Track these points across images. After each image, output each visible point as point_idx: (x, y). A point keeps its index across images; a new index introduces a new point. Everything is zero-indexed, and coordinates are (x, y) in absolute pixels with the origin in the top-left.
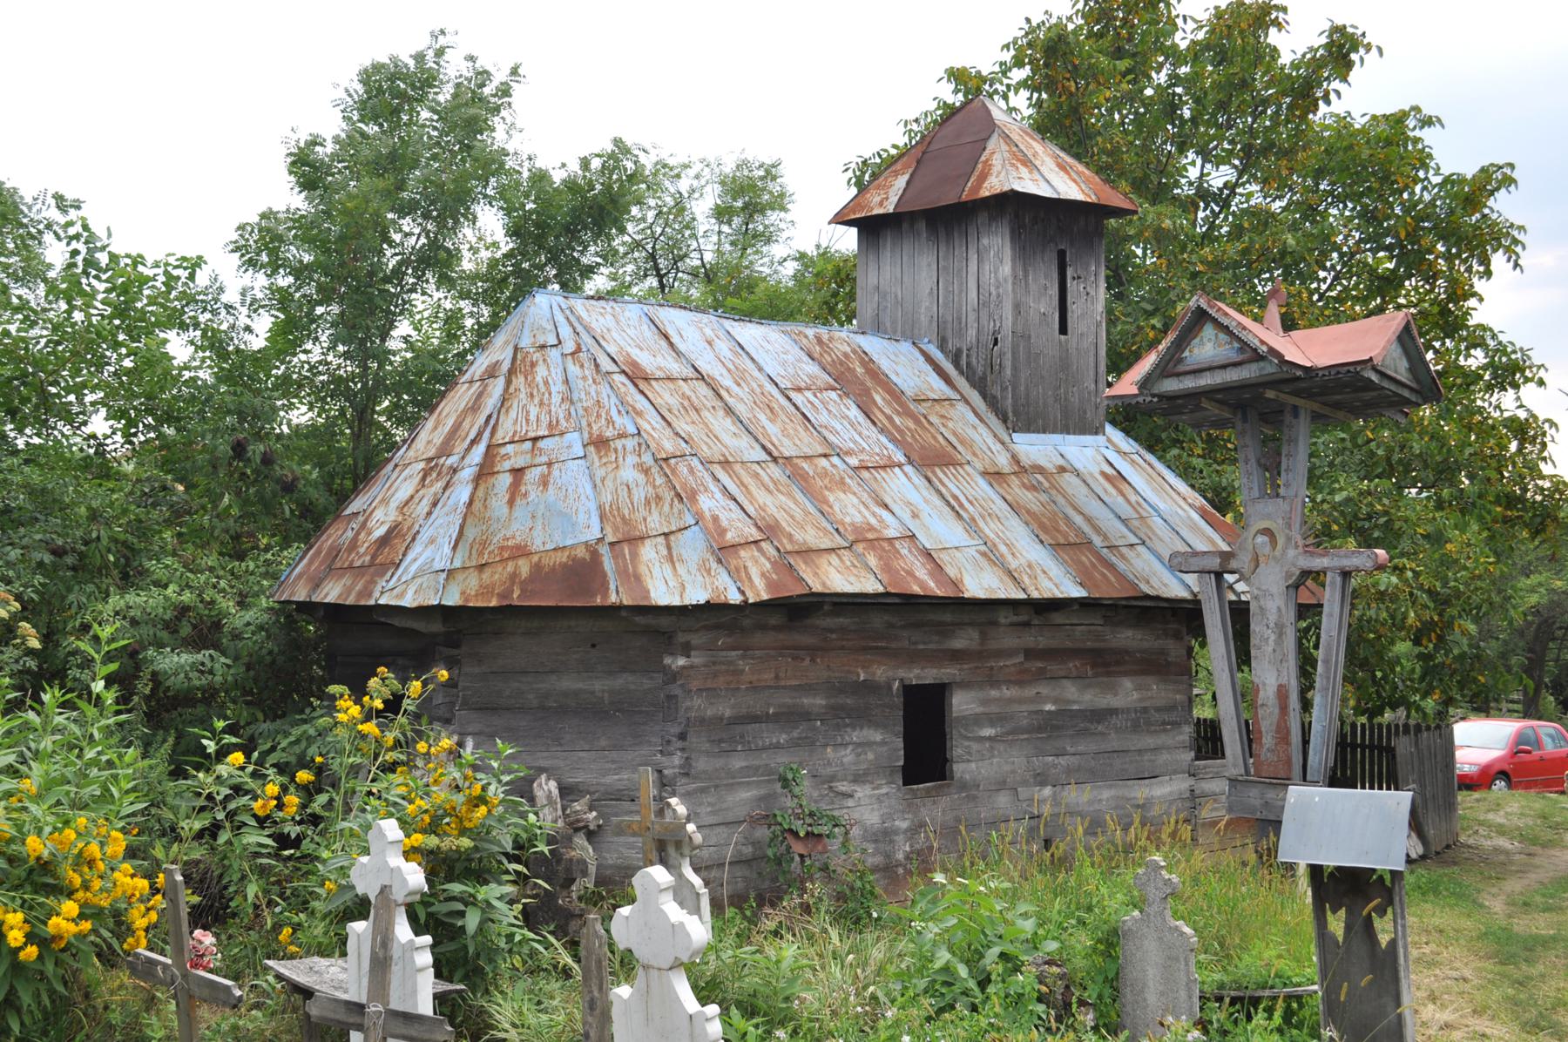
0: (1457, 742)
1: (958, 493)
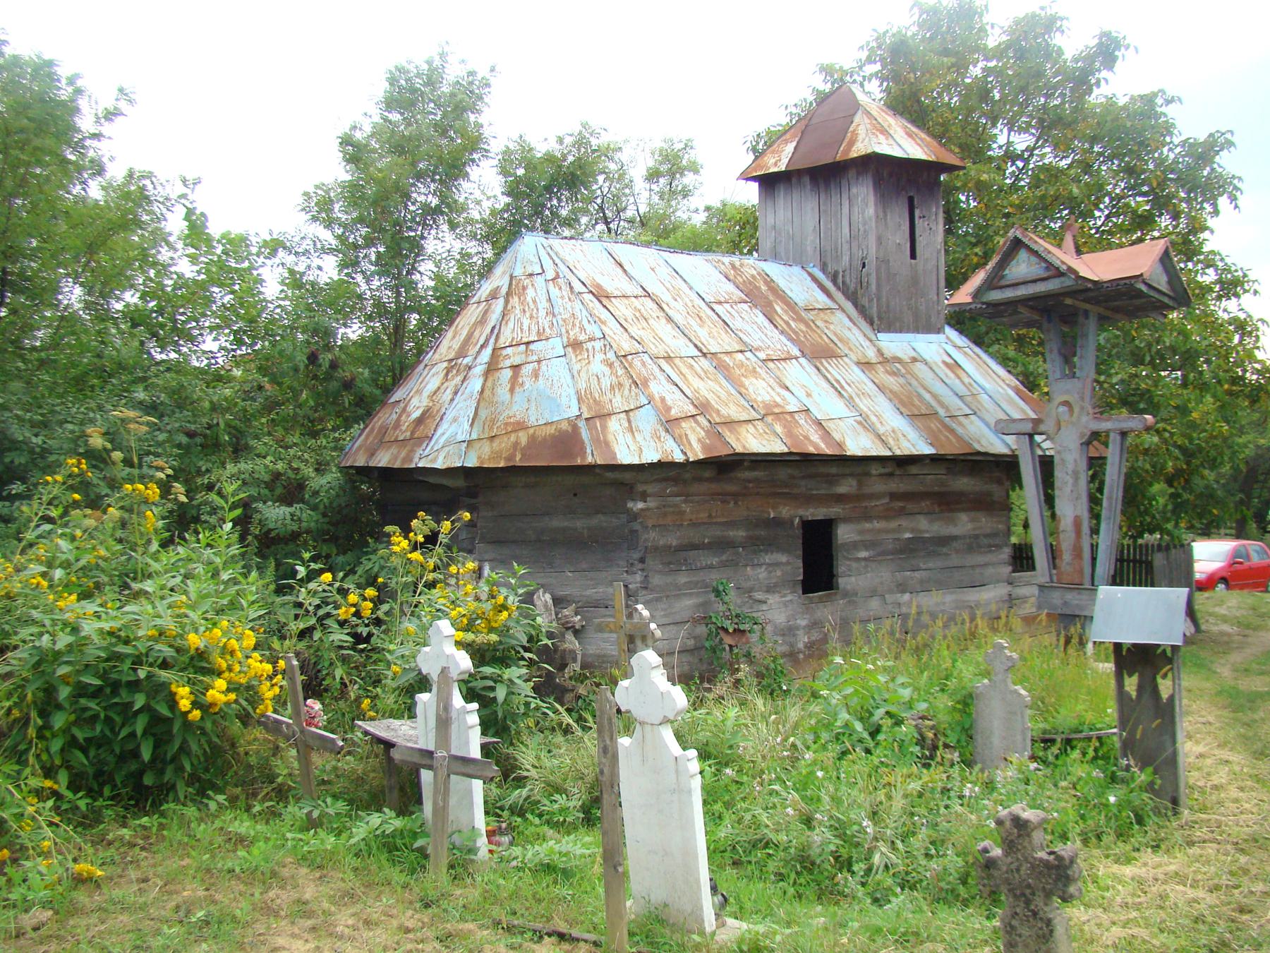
0: (1196, 556)
1: (839, 378)
